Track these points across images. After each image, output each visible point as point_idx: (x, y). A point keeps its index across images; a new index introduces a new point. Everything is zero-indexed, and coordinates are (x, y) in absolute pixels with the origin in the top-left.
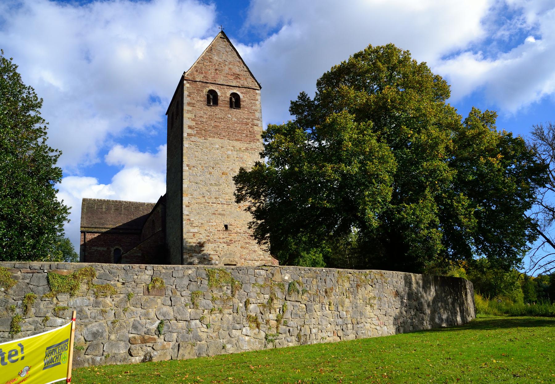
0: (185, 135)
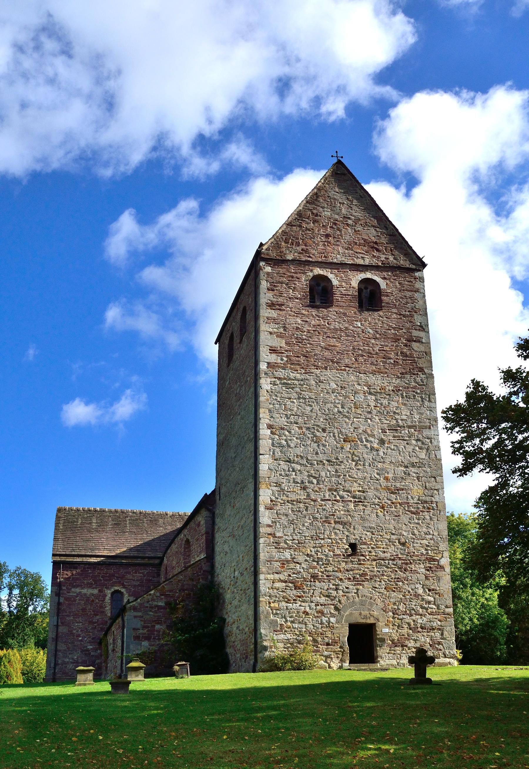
0: (263, 366)
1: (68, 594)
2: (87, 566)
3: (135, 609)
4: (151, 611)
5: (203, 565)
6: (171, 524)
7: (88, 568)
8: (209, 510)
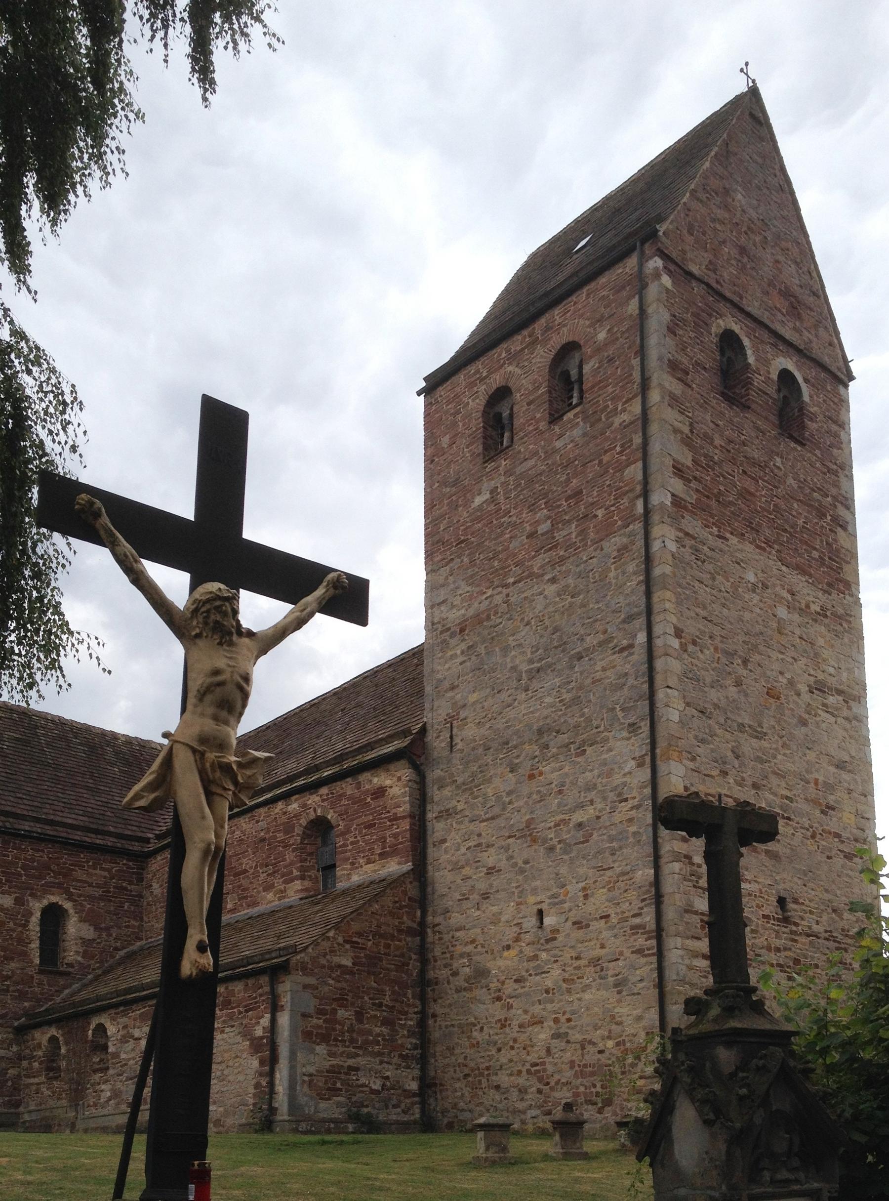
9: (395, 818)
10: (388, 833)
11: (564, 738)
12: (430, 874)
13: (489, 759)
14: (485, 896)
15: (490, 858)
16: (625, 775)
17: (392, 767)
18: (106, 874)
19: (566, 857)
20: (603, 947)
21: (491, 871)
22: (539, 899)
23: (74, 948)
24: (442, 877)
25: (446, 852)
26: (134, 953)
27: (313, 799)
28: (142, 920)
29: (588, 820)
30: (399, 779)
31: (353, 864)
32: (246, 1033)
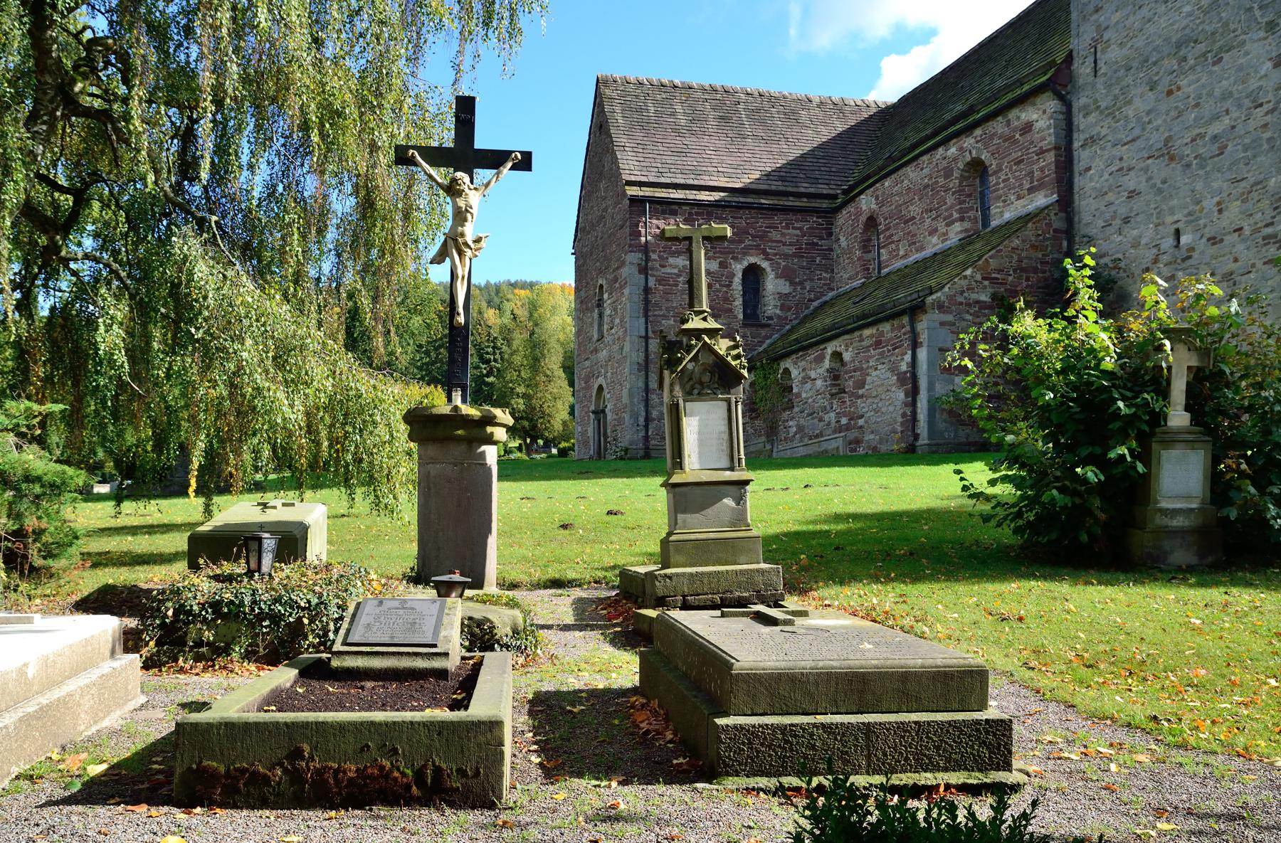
1: (663, 270)
2: (696, 210)
3: (940, 307)
4: (968, 312)
5: (1053, 218)
6: (824, 124)
7: (697, 214)
8: (1062, 98)
9: (1041, 152)
10: (1035, 167)
11: (1201, 48)
12: (1077, 203)
13: (1129, 80)
14: (1126, 220)
15: (1131, 182)
16: (1261, 78)
17: (1038, 100)
18: (798, 232)
19: (1201, 172)
20: (1236, 260)
21: (1132, 194)
22: (1176, 218)
23: (772, 303)
24: (1087, 206)
25: (1091, 180)
26: (826, 303)
27: (968, 142)
28: (832, 271)
29: (1224, 131)
30: (1044, 112)
31: (1004, 201)
32: (894, 369)
